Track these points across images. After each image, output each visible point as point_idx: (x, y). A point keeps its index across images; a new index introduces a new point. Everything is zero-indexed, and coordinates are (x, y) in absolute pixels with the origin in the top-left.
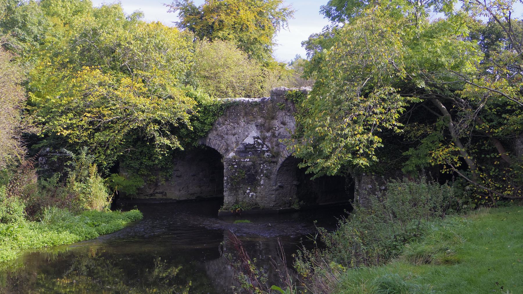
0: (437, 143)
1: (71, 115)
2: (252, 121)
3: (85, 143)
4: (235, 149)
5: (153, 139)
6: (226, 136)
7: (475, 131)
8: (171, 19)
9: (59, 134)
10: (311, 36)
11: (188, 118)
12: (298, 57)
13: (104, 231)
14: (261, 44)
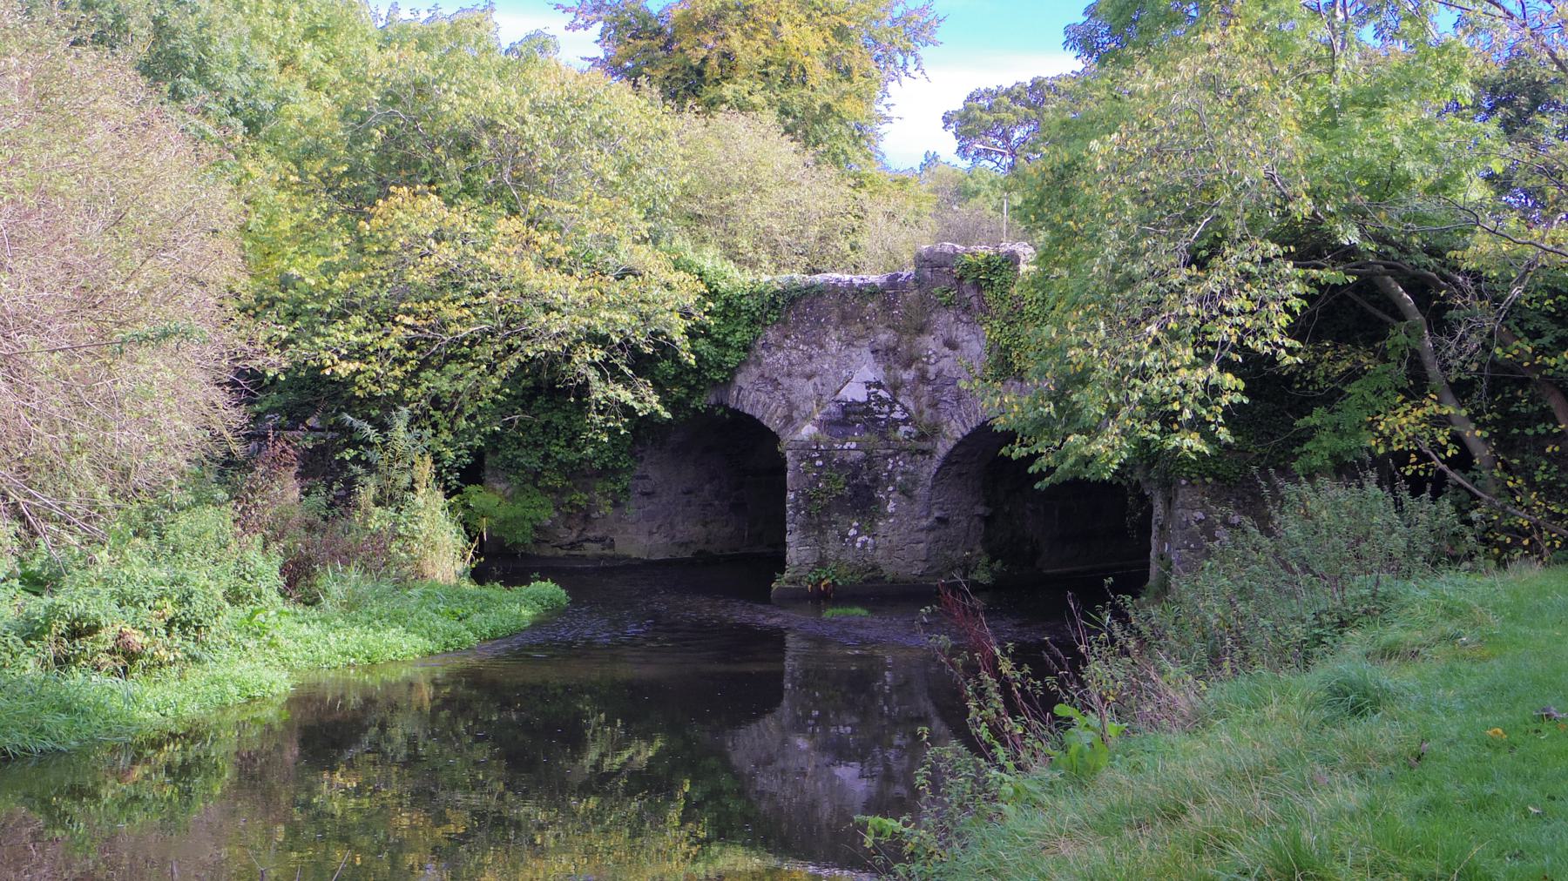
0: (1389, 393)
1: (358, 321)
3: (398, 399)
4: (818, 417)
5: (584, 389)
6: (786, 382)
7: (1494, 364)
8: (580, 46)
9: (328, 372)
10: (971, 98)
12: (931, 160)
13: (486, 631)
14: (842, 121)
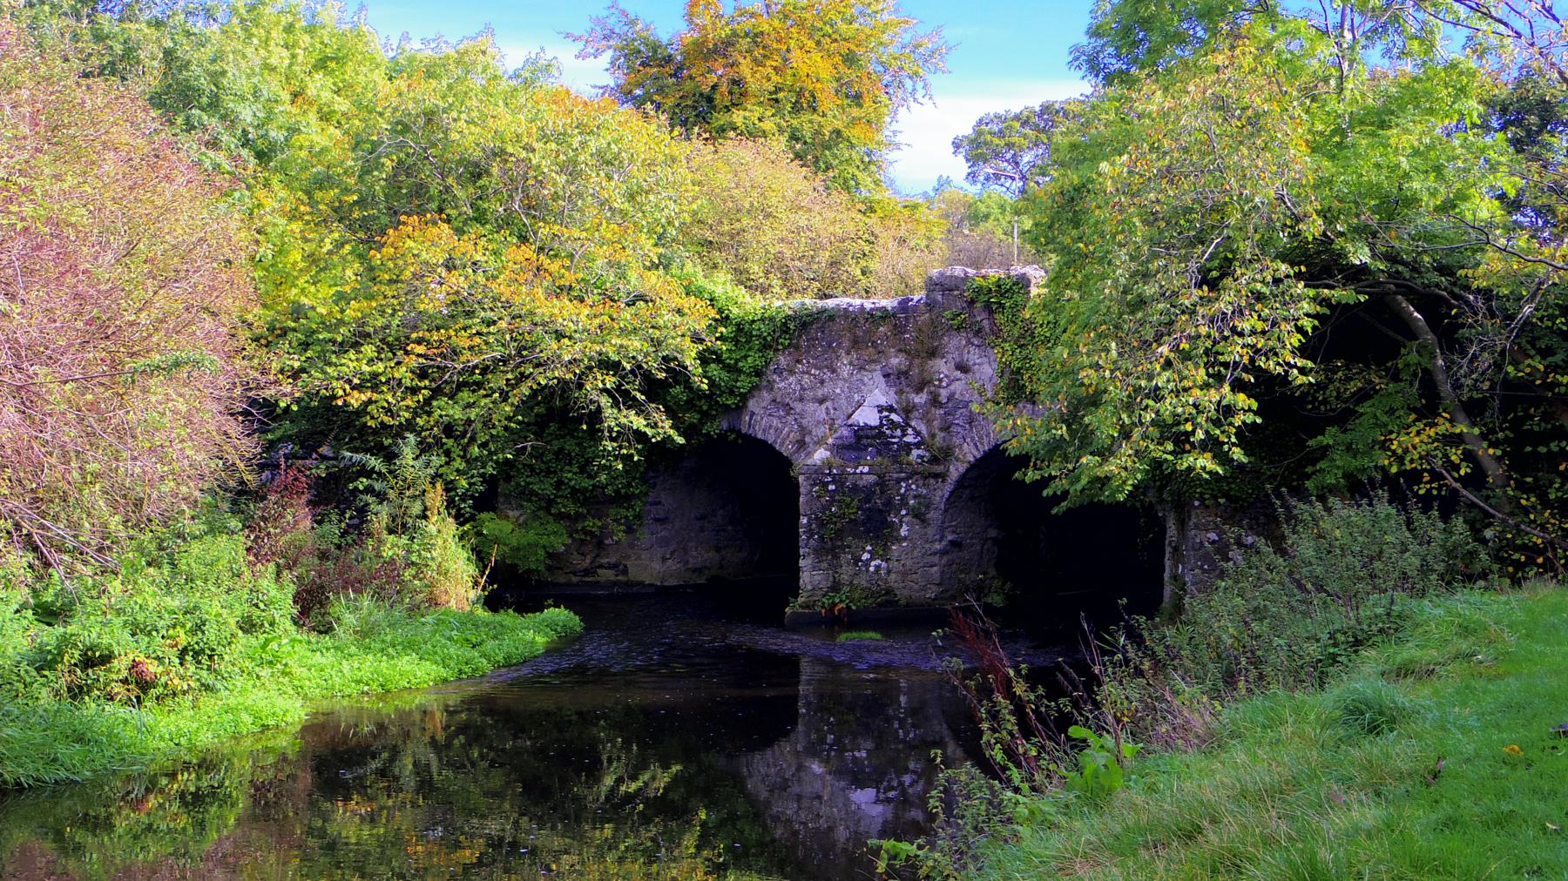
1: (369, 350)
2: (874, 361)
4: (830, 441)
5: (596, 416)
6: (798, 406)
8: (589, 74)
11: (693, 355)
13: (500, 658)
